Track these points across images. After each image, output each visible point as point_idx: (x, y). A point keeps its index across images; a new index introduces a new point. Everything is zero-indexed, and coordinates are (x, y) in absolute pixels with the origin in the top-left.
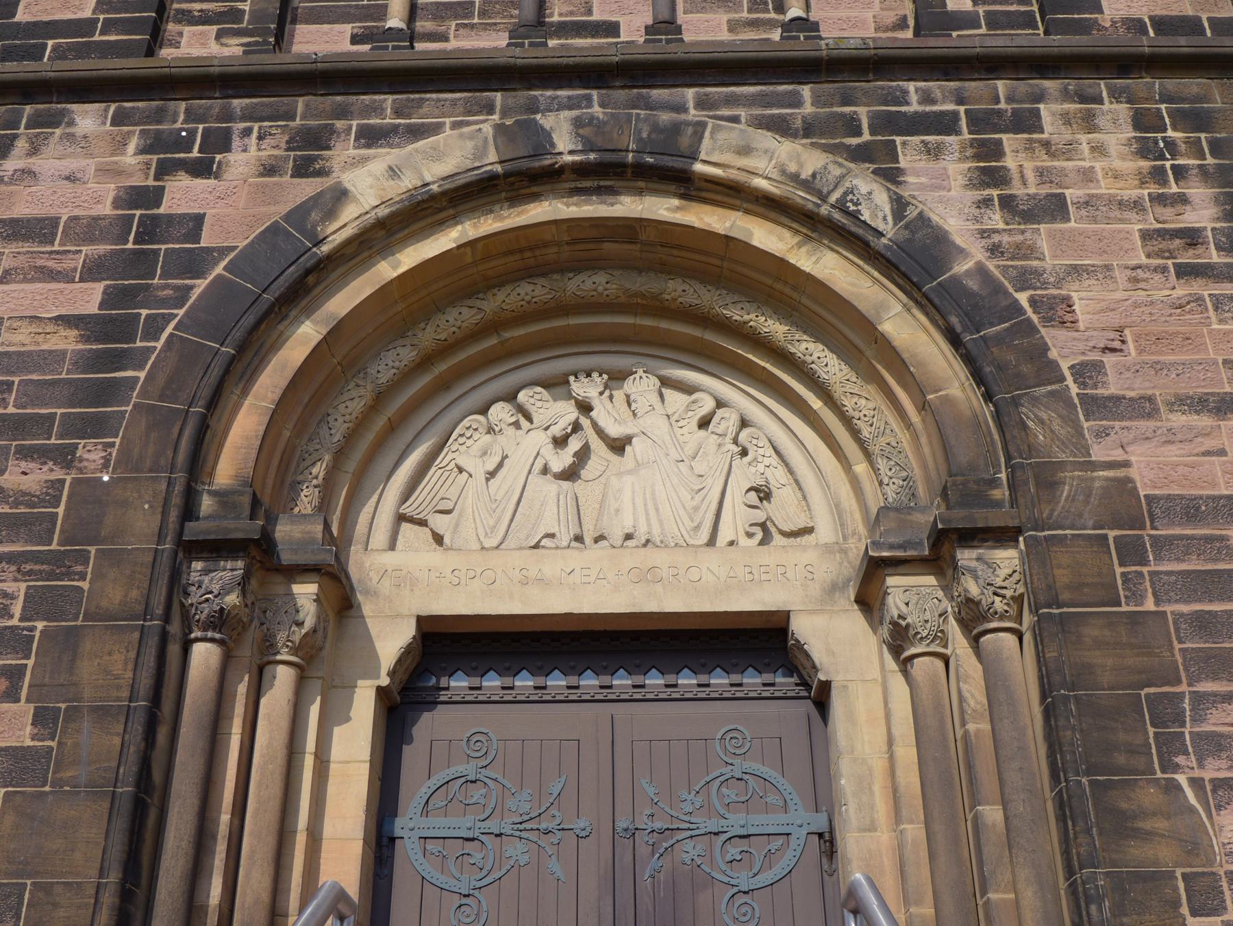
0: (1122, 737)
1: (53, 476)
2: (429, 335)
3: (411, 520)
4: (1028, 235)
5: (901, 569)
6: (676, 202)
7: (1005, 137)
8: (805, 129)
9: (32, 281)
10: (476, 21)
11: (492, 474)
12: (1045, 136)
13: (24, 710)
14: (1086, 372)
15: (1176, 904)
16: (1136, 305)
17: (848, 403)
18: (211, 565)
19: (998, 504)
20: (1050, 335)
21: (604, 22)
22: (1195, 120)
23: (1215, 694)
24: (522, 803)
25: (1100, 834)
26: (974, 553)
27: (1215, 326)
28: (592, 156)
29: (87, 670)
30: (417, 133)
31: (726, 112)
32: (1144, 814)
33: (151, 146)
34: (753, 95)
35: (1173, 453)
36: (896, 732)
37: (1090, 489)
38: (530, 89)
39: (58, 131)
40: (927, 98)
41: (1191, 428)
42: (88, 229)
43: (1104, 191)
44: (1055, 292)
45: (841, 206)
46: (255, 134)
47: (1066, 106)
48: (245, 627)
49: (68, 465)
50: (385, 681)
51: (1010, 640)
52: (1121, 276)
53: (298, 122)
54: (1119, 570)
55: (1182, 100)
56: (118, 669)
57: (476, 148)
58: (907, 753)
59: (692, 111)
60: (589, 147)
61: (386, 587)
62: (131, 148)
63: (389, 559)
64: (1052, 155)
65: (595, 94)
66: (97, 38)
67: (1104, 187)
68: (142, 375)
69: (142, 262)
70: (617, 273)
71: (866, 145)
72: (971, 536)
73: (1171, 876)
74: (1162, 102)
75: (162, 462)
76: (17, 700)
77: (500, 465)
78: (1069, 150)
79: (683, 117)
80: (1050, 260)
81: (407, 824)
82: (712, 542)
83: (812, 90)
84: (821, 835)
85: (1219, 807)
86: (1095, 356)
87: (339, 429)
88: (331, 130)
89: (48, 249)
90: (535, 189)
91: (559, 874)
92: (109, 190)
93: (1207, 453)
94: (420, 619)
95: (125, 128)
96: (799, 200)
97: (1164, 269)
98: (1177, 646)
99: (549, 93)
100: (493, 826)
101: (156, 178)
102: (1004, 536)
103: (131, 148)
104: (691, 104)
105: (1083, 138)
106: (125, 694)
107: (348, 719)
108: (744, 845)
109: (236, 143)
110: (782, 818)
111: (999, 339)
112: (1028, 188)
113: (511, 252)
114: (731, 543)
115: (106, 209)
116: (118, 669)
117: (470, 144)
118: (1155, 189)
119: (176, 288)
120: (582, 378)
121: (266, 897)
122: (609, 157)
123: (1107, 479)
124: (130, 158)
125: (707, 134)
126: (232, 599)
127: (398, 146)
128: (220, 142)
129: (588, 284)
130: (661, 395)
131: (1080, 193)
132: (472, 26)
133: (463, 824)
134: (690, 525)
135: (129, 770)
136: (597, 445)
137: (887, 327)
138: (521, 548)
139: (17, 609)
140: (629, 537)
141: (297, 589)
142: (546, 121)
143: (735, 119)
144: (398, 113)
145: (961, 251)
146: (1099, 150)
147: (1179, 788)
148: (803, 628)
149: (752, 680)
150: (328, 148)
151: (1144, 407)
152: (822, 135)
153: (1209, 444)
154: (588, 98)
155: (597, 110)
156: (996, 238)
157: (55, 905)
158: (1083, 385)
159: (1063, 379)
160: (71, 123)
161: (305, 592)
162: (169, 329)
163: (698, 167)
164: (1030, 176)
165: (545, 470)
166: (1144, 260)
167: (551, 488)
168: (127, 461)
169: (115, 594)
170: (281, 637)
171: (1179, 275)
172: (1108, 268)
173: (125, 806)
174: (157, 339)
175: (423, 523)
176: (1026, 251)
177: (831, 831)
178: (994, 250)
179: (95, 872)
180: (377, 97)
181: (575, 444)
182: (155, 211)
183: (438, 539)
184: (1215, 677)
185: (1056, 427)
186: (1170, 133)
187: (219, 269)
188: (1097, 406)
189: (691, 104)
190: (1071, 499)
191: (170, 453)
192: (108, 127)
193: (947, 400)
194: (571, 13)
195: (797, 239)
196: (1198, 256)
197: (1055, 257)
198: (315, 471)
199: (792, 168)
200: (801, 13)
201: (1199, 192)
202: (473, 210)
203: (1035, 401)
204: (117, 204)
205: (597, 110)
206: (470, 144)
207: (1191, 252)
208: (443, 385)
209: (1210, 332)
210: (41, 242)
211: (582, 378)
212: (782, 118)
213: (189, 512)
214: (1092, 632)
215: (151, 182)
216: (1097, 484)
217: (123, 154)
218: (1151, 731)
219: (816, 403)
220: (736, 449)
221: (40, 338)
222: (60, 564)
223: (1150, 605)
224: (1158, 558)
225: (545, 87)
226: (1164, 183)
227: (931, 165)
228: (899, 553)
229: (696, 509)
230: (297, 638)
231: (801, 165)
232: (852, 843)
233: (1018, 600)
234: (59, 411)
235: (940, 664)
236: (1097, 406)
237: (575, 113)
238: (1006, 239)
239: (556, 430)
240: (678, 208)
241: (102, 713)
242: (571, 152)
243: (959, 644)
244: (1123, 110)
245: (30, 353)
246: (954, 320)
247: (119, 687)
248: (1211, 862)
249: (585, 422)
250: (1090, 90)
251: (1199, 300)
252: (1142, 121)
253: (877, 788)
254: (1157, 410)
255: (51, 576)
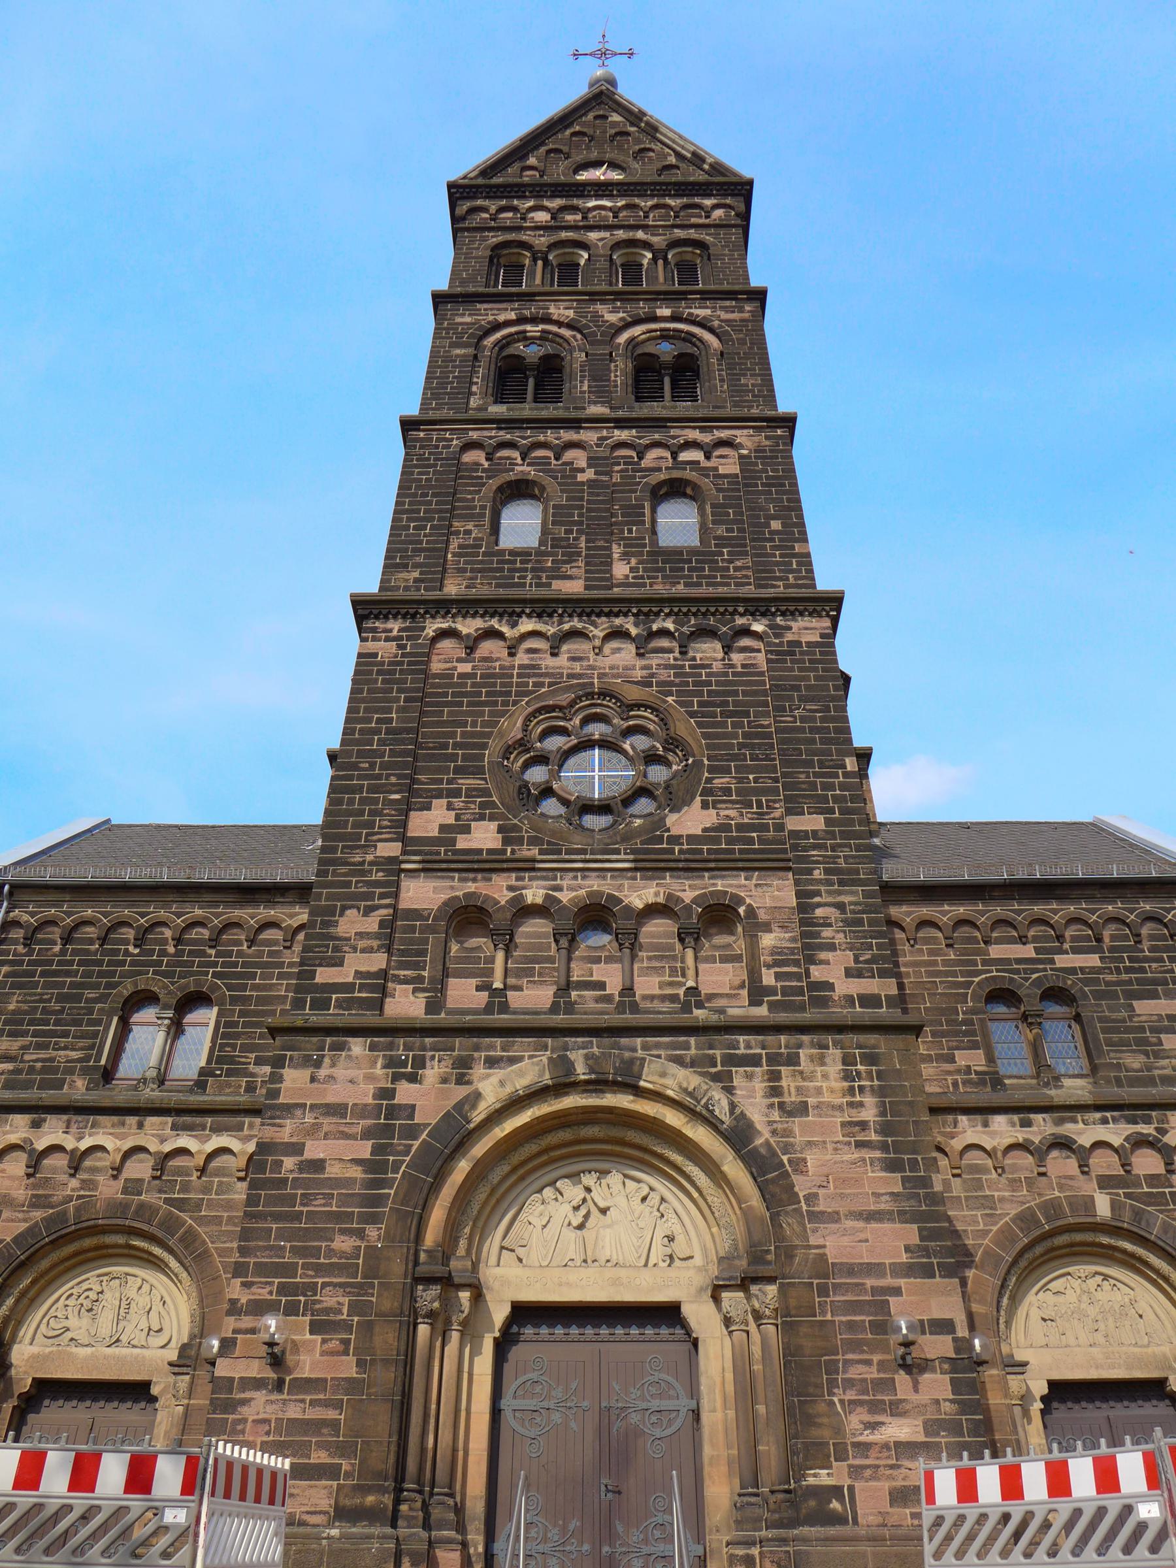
0: (813, 1379)
1: (356, 1244)
2: (516, 1158)
3: (507, 1249)
4: (790, 1124)
5: (728, 1289)
6: (631, 1098)
7: (782, 1068)
8: (691, 1063)
9: (338, 1139)
10: (536, 979)
11: (545, 1226)
12: (801, 1068)
13: (351, 1359)
14: (811, 1198)
15: (829, 1456)
16: (835, 1163)
17: (709, 1199)
18: (426, 1287)
19: (769, 1263)
20: (795, 1178)
21: (599, 981)
22: (871, 1059)
23: (853, 1360)
24: (558, 1393)
25: (801, 1424)
26: (758, 1287)
27: (870, 1174)
28: (593, 1076)
29: (378, 1341)
30: (513, 1060)
31: (655, 1052)
32: (819, 1415)
33: (388, 1064)
34: (668, 1043)
35: (845, 1241)
36: (725, 1365)
37: (808, 1259)
38: (565, 1036)
39: (343, 1053)
40: (748, 1046)
41: (854, 1228)
42: (362, 1111)
43: (826, 1099)
44: (799, 1155)
45: (706, 1106)
46: (437, 1059)
47: (812, 1051)
48: (439, 1314)
49: (362, 1239)
50: (497, 1334)
51: (772, 1328)
52: (830, 1146)
53: (456, 1053)
54: (817, 1300)
55: (866, 1047)
56: (390, 1341)
57: (539, 1070)
58: (729, 1376)
59: (640, 1051)
60: (592, 1071)
61: (497, 1286)
62: (379, 1065)
63: (498, 1271)
64: (804, 1079)
65: (594, 1040)
66: (356, 995)
67: (826, 1098)
68: (392, 1192)
69: (387, 1130)
70: (604, 1126)
71: (719, 1072)
72: (756, 1280)
73: (828, 1443)
74: (856, 1048)
75: (404, 1238)
76: (349, 1355)
77: (549, 1221)
78: (811, 1078)
79: (635, 1055)
80: (799, 1139)
81: (506, 1403)
82: (646, 1265)
83: (695, 1041)
84: (693, 1411)
85: (850, 1413)
86: (814, 1190)
87: (476, 1207)
88: (472, 1058)
89: (344, 1121)
90: (566, 1090)
91: (575, 1429)
92: (371, 1089)
93: (860, 1241)
94: (512, 1302)
95: (375, 1053)
96: (687, 1103)
97: (849, 1143)
98: (839, 1337)
99: (573, 1039)
100: (545, 1404)
101: (392, 1083)
102: (771, 1280)
103: (379, 1065)
104: (639, 1047)
105: (819, 1069)
106: (395, 1353)
107: (481, 1354)
108: (658, 1415)
109: (428, 1064)
110: (676, 1402)
111: (773, 1181)
112: (791, 1098)
113: (555, 1118)
114: (655, 1265)
115: (370, 1100)
116: (390, 1341)
117: (537, 1068)
118: (848, 1099)
119: (405, 1145)
120: (587, 1173)
121: (451, 1443)
122: (602, 1077)
123: (816, 1254)
124: (379, 1071)
125: (646, 1065)
126: (436, 1305)
127: (504, 1068)
128: (420, 1063)
129: (591, 1132)
130: (624, 1183)
131: (815, 1100)
132: (534, 982)
133: (530, 1404)
134: (636, 1255)
135: (398, 1388)
136: (594, 1210)
137: (725, 1168)
138: (558, 1266)
139: (345, 1311)
140: (608, 1261)
141: (461, 1294)
142: (572, 1055)
143: (659, 1057)
144: (503, 1050)
145: (759, 1132)
146: (825, 1076)
147: (834, 1403)
148: (687, 1310)
149: (664, 1331)
150: (471, 1068)
151: (834, 1217)
152: (699, 1067)
153: (862, 1236)
154: (591, 1042)
155: (595, 1050)
156: (775, 1126)
157: (372, 1451)
158: (808, 1205)
159: (800, 1202)
160: (350, 1049)
161: (465, 1296)
162: (403, 1168)
163: (642, 1083)
164: (793, 1090)
165: (569, 1224)
166: (841, 1138)
167: (571, 1235)
168: (388, 1237)
169: (388, 1304)
170: (454, 1318)
171: (856, 1146)
172: (824, 1142)
173: (397, 1405)
174: (398, 1173)
175: (513, 1251)
176: (788, 1133)
177: (698, 1409)
178: (774, 1132)
179: (387, 1436)
180: (492, 1039)
181: (583, 1211)
182: (392, 1102)
183: (520, 1260)
184: (854, 1352)
185: (795, 1227)
186: (859, 1067)
187: (424, 1136)
188: (815, 1216)
189: (639, 1047)
190: (799, 1264)
191: (407, 1233)
192: (367, 1052)
193: (750, 1207)
194: (583, 975)
195: (687, 1119)
196: (866, 1136)
197: (800, 1136)
198: (465, 1231)
199: (685, 1085)
200: (693, 984)
201: (869, 1100)
202: (538, 1100)
203: (787, 1213)
204: (375, 1097)
205: (595, 1050)
206: (537, 1068)
207: (863, 1134)
208: (522, 1178)
209: (867, 1177)
210: (341, 1117)
211: (587, 1173)
212: (681, 1056)
213: (416, 1263)
214: (804, 1330)
215: (389, 1085)
216: (811, 1257)
217: (376, 1068)
218: (825, 1377)
219: (696, 1195)
220: (660, 1215)
221: (345, 1170)
222: (362, 1288)
223: (829, 1317)
224: (834, 1294)
225: (571, 1037)
226: (853, 1095)
227: (748, 1084)
228: (728, 1283)
229: (640, 1247)
230: (461, 1319)
231: (689, 1084)
232: (705, 1417)
233: (776, 1310)
234: (357, 1210)
235: (745, 1335)
236: (815, 1216)
237: (585, 1051)
238: (779, 1126)
239: (575, 1203)
240: (633, 1101)
241: (386, 1362)
242: (584, 1074)
243: (752, 1327)
244: (838, 1053)
245: (340, 1178)
246: (754, 1170)
247: (392, 1350)
248: (845, 1438)
249: (588, 1197)
250: (824, 1042)
251: (864, 1160)
252: (847, 1060)
253: (717, 1391)
254: (840, 1219)
255: (359, 1295)
